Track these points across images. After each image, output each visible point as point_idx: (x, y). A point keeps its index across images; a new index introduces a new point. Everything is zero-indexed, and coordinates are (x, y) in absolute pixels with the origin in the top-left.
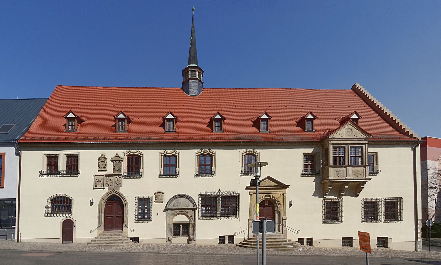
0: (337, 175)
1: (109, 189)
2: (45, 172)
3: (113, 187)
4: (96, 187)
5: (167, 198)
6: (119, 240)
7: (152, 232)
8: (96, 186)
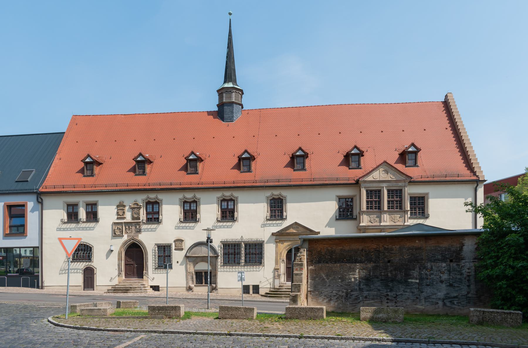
0: (370, 221)
1: (128, 236)
2: (66, 220)
3: (133, 234)
4: (115, 235)
5: (187, 245)
6: (139, 287)
7: (173, 281)
8: (115, 234)
